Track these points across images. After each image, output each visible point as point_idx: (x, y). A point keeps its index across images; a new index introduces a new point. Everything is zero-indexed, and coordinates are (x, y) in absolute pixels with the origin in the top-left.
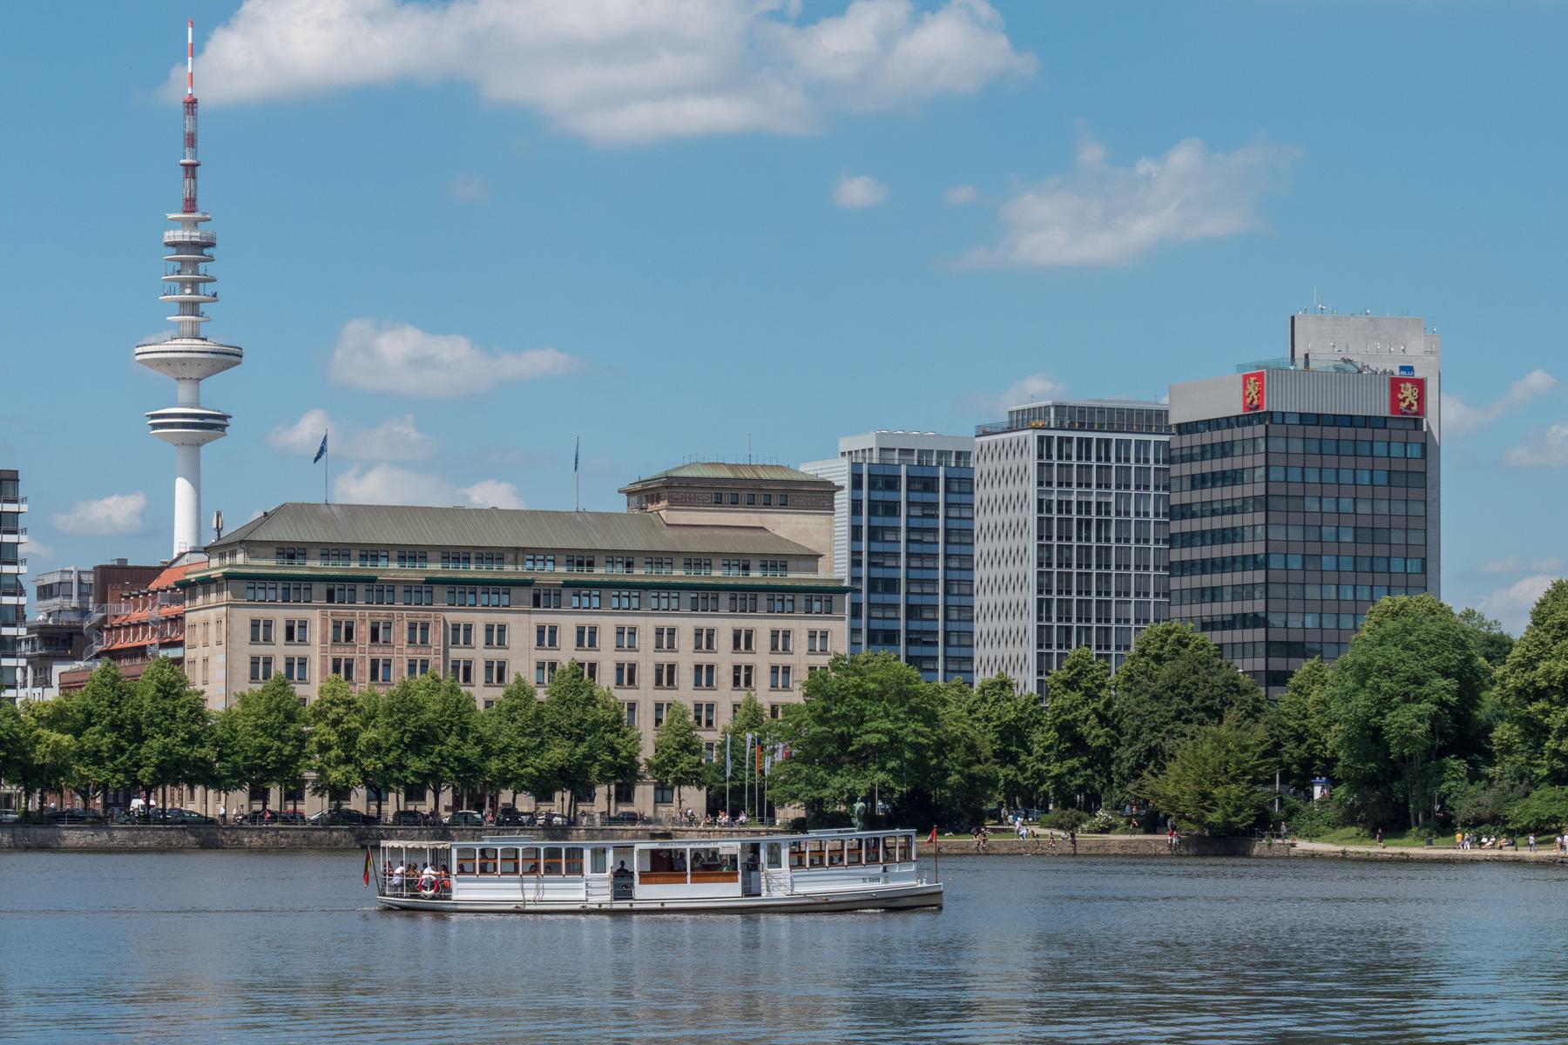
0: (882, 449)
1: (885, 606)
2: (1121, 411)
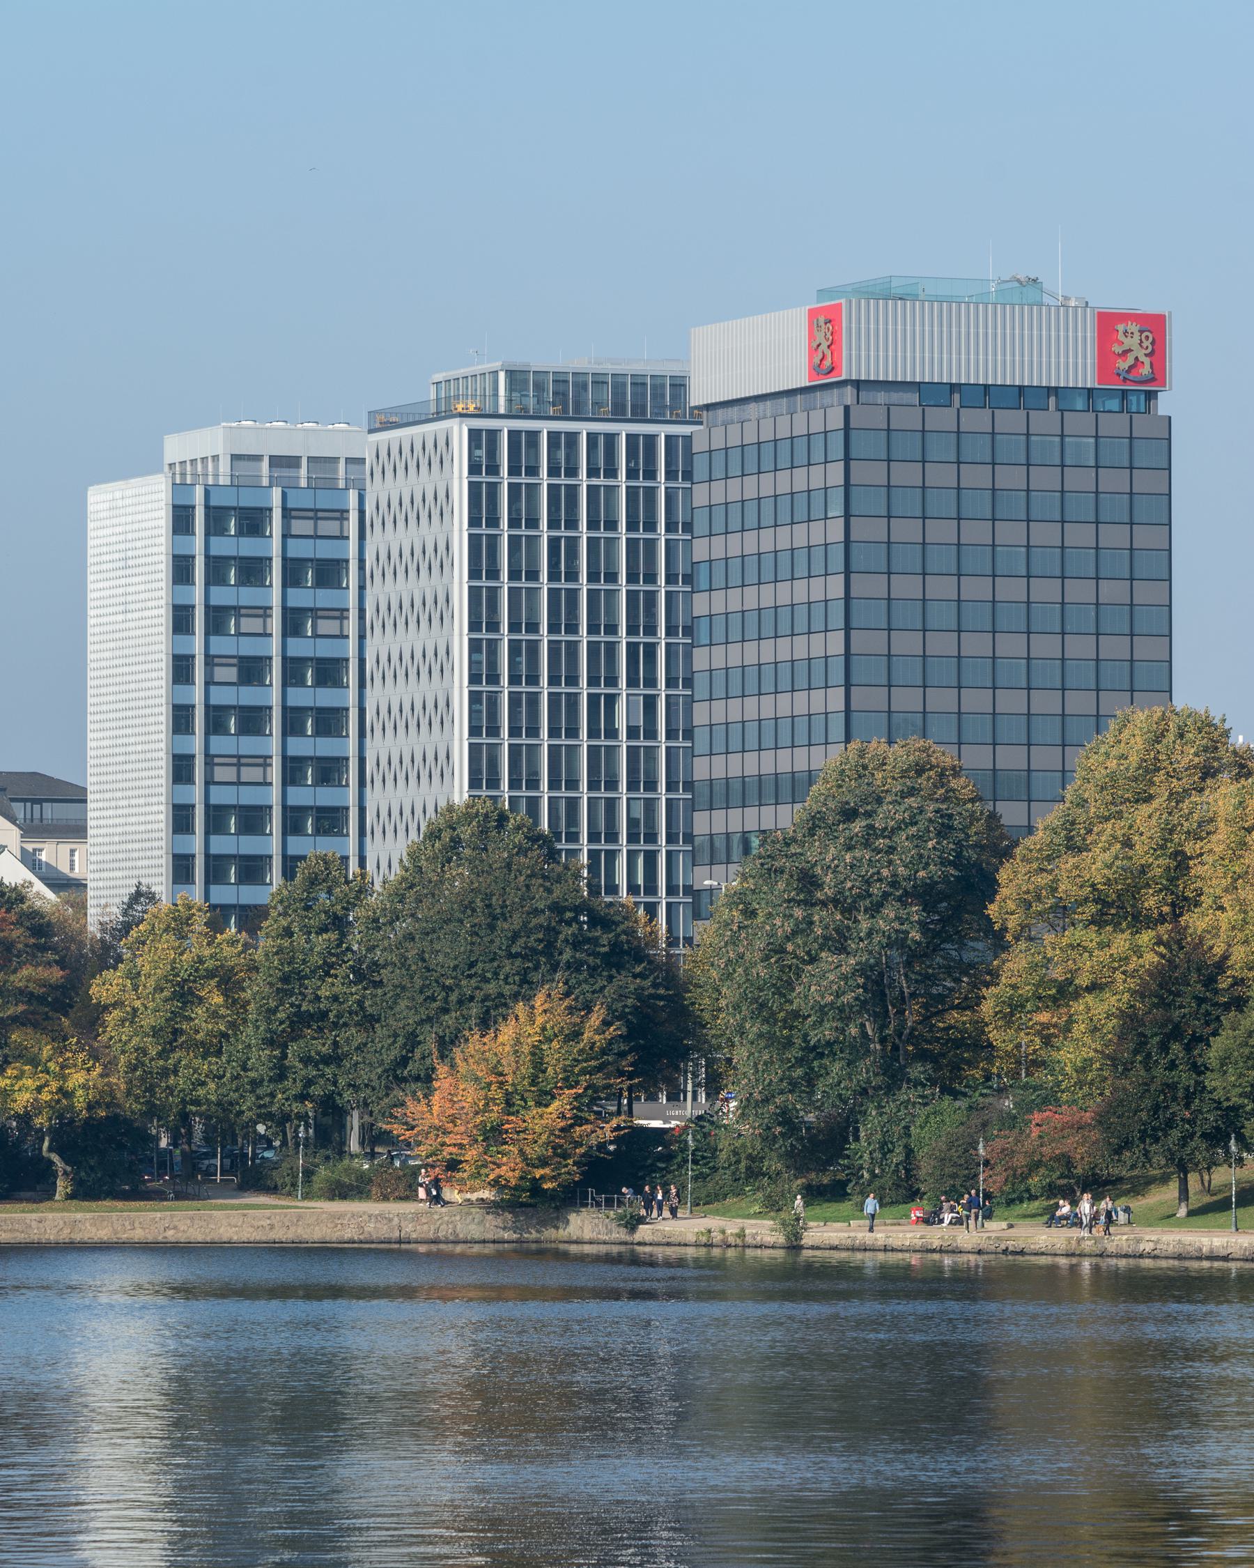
0: (235, 458)
1: (239, 761)
2: (639, 383)
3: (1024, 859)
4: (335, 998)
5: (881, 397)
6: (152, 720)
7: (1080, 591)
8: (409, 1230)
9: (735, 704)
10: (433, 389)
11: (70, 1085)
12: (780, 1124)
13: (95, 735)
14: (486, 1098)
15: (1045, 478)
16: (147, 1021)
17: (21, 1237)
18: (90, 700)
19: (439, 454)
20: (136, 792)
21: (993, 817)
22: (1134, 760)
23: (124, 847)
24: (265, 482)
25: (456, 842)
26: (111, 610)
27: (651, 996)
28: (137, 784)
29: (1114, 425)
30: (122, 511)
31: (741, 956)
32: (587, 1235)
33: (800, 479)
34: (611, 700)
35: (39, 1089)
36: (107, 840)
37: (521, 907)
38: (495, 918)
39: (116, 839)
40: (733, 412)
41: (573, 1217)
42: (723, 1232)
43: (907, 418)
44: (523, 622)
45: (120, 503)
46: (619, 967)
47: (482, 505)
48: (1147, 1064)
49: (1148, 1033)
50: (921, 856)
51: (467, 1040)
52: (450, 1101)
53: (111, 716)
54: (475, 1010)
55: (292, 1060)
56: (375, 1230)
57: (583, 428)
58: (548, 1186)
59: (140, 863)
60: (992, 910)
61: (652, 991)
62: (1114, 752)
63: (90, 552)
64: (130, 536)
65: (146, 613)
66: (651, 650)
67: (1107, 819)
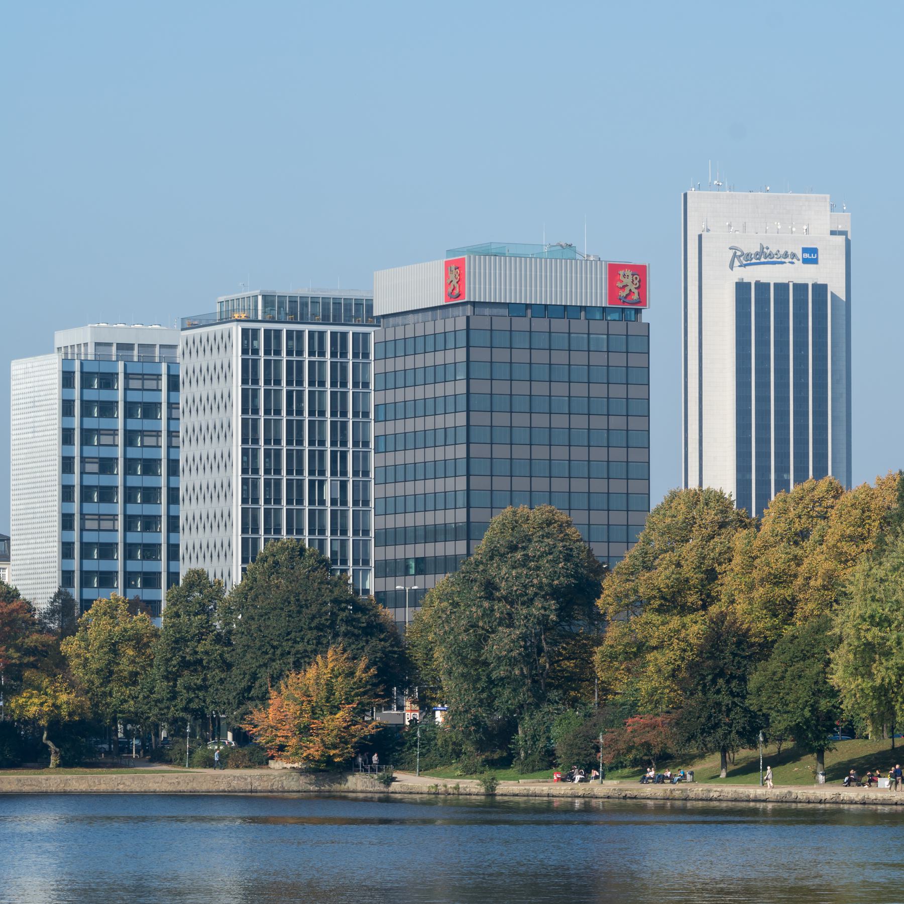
1: (100, 517)
2: (337, 303)
3: (618, 573)
4: (206, 653)
5: (487, 311)
6: (50, 494)
7: (598, 422)
8: (257, 785)
9: (400, 486)
10: (218, 305)
11: (58, 702)
12: (473, 725)
13: (15, 502)
14: (301, 709)
15: (579, 358)
16: (94, 666)
17: (36, 789)
18: (12, 483)
19: (225, 342)
20: (40, 535)
21: (590, 551)
22: (681, 518)
23: (32, 566)
24: (114, 358)
25: (276, 563)
26: (25, 431)
27: (390, 652)
28: (40, 530)
29: (618, 328)
30: (32, 374)
31: (452, 629)
32: (359, 788)
33: (440, 358)
34: (322, 483)
35: (42, 704)
36: (22, 562)
37: (309, 602)
38: (301, 607)
39: (28, 562)
40: (399, 320)
41: (350, 778)
42: (445, 786)
43: (501, 324)
44: (272, 438)
45: (30, 370)
46: (372, 635)
47: (249, 372)
48: (704, 692)
49: (705, 673)
50: (556, 572)
51: (288, 676)
52: (277, 713)
53: (25, 491)
54: (291, 659)
55: (179, 687)
56: (236, 785)
57: (306, 328)
58: (337, 760)
59: (42, 576)
60: (599, 603)
61: (390, 649)
62: (668, 513)
63: (12, 398)
64: (36, 389)
65: (46, 433)
66: (344, 455)
67: (666, 551)
